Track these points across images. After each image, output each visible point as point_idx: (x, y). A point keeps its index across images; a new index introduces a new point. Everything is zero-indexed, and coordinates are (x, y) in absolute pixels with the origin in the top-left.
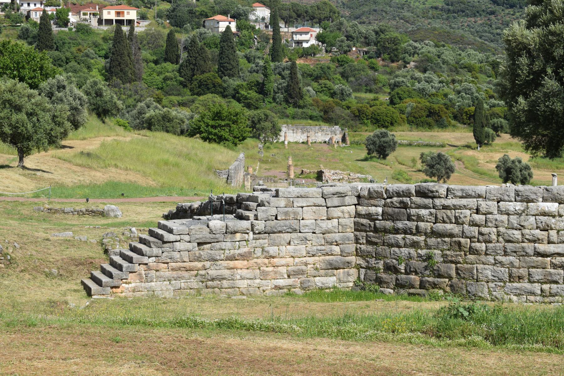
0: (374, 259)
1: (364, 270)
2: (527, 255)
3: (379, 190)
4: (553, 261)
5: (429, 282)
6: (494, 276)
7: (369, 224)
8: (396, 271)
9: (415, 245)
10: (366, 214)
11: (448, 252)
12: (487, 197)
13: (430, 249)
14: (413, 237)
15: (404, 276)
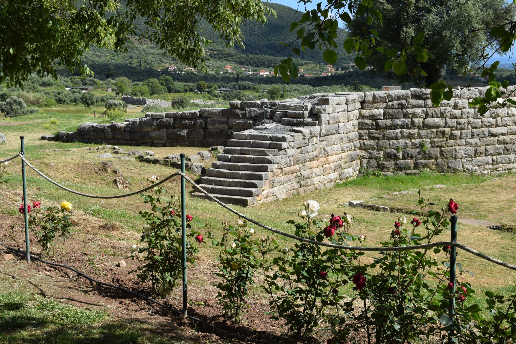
0: (375, 150)
1: (366, 160)
2: (485, 136)
3: (383, 95)
4: (499, 139)
5: (422, 163)
6: (466, 154)
7: (372, 123)
8: (396, 157)
9: (410, 136)
10: (370, 116)
11: (435, 140)
12: (462, 96)
13: (422, 138)
14: (408, 130)
15: (402, 161)
